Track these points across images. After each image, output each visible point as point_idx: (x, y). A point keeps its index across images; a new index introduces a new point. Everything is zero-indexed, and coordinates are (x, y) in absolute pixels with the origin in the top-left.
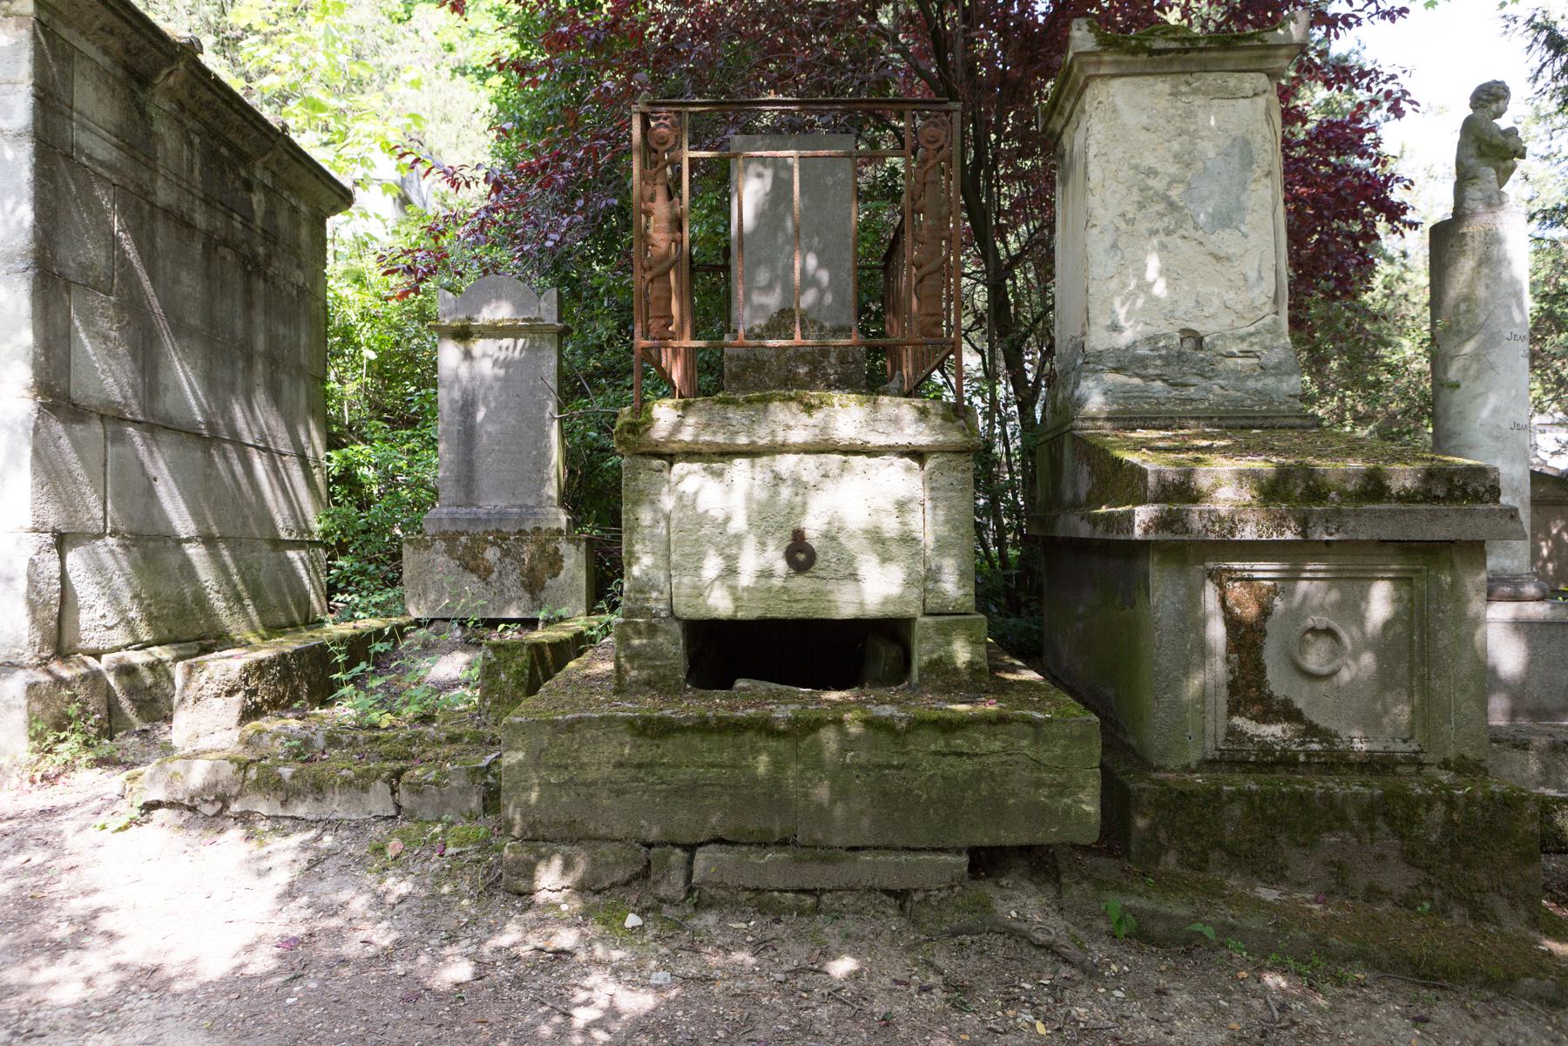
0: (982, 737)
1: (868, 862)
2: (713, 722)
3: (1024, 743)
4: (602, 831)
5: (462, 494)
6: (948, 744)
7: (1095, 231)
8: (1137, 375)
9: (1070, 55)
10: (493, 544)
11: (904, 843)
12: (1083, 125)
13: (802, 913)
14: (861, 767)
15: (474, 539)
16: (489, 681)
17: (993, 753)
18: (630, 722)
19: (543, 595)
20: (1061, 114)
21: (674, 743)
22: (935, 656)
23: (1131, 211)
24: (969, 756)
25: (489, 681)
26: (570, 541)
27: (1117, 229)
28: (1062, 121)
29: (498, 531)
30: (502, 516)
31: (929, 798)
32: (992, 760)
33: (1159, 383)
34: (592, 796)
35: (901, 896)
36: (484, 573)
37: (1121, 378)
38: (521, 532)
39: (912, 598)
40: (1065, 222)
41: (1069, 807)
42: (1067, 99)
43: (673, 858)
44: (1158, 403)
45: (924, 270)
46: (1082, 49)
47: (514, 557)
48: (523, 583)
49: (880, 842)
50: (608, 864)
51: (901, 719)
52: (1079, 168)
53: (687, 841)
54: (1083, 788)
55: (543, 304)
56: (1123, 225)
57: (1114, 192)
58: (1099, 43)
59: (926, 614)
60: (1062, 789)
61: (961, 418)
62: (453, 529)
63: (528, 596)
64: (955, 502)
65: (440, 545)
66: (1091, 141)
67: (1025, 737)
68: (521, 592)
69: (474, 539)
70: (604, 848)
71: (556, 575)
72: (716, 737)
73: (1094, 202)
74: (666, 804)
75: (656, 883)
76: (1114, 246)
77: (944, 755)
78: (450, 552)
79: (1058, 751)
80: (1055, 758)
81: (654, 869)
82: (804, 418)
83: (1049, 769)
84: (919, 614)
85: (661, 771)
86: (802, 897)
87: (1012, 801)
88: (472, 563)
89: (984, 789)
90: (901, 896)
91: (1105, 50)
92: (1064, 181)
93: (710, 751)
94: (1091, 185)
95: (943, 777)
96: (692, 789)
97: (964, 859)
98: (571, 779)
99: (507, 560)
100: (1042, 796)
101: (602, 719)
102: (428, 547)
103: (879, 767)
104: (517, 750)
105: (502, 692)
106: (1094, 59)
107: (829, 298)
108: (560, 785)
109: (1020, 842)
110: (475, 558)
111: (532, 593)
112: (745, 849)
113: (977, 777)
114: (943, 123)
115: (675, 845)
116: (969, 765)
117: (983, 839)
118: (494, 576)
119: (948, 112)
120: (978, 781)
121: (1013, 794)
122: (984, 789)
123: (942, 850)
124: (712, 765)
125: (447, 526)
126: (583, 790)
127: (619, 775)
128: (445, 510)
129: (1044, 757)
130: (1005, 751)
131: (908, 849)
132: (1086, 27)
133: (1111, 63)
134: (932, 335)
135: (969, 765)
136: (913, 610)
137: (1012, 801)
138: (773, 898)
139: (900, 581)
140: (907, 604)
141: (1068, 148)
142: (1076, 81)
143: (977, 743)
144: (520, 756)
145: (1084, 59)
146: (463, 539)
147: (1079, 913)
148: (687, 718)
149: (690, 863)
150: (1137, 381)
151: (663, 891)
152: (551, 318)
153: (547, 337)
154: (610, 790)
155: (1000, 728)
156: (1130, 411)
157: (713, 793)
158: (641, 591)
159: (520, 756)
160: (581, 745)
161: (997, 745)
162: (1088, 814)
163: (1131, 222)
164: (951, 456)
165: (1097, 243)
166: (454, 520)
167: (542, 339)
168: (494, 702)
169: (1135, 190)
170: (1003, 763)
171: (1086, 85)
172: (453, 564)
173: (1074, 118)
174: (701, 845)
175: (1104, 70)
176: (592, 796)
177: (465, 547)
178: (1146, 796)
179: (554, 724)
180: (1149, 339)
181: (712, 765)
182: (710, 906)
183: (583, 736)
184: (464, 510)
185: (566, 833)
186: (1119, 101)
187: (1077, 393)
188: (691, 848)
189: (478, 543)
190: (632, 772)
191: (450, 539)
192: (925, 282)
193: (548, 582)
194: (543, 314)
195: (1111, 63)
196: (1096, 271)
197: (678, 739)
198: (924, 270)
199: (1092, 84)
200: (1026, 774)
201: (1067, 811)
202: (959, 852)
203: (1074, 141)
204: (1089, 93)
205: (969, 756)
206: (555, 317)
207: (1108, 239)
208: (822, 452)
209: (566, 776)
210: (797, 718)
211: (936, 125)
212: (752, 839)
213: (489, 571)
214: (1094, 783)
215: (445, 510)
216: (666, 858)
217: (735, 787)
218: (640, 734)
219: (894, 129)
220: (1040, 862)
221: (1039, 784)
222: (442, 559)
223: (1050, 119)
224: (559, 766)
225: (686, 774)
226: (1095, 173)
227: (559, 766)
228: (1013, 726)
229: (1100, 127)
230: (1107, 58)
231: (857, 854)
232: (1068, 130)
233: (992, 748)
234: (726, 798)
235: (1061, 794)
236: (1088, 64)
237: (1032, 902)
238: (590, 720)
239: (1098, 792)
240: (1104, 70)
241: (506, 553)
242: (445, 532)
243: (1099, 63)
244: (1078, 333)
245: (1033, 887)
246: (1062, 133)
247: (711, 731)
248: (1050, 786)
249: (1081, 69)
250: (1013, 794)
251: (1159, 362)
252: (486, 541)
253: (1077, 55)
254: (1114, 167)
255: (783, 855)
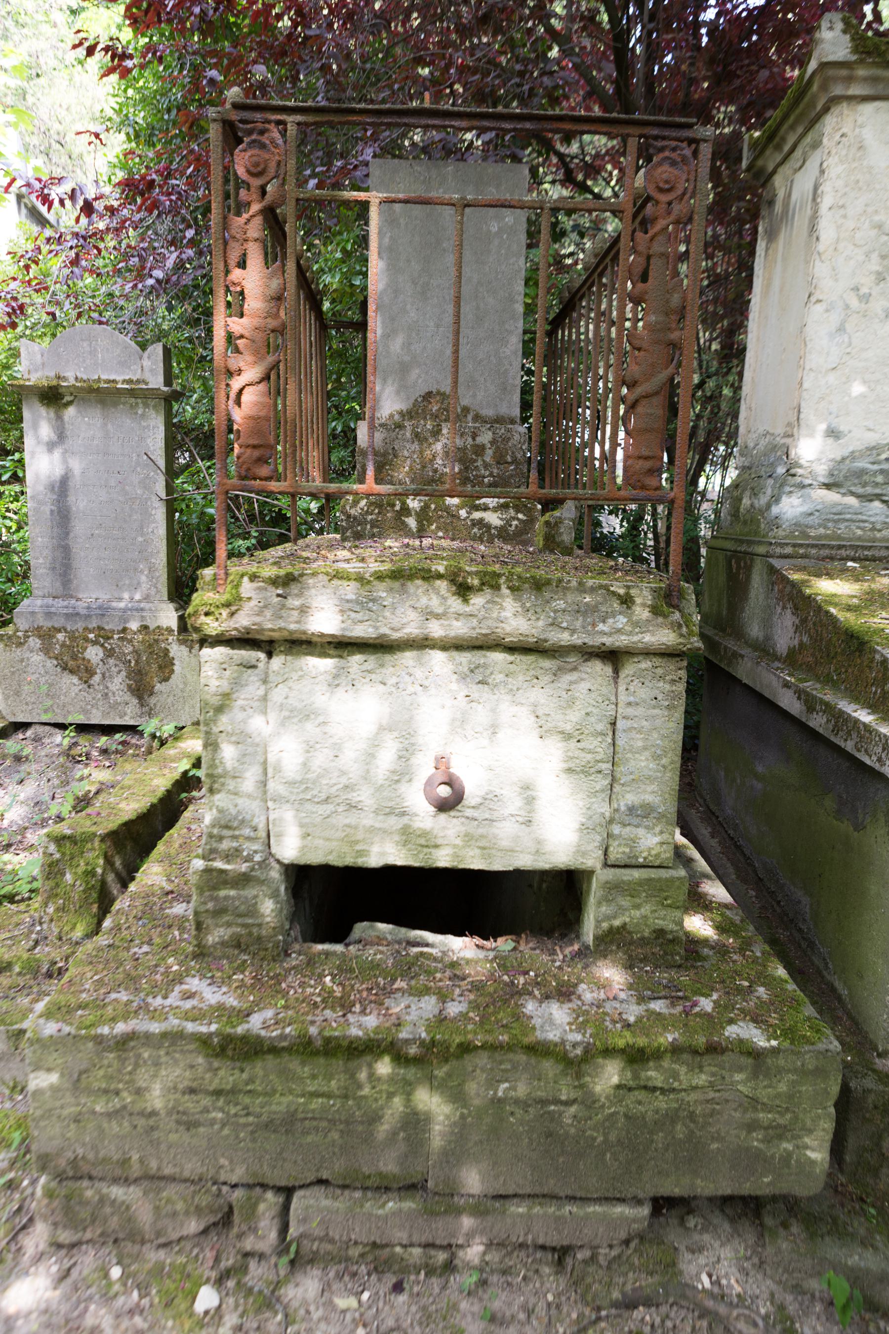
0: (683, 1070)
1: (521, 1216)
2: (319, 1043)
3: (738, 1077)
4: (168, 1171)
5: (58, 584)
6: (636, 1077)
7: (819, 308)
8: (852, 494)
9: (813, 65)
10: (95, 643)
11: (569, 1192)
12: (812, 165)
13: (431, 1271)
14: (517, 1101)
15: (72, 636)
16: (51, 883)
17: (695, 1088)
18: (204, 1041)
19: (152, 701)
20: (779, 147)
21: (259, 1068)
22: (617, 923)
23: (867, 283)
24: (663, 1091)
25: (51, 883)
26: (182, 642)
27: (847, 307)
28: (779, 157)
29: (100, 628)
30: (104, 611)
31: (606, 1141)
32: (693, 1096)
33: (877, 504)
34: (152, 1129)
35: (561, 1254)
36: (85, 672)
37: (832, 497)
38: (124, 630)
39: (590, 847)
40: (767, 286)
41: (789, 1154)
42: (792, 128)
43: (262, 1207)
44: (873, 529)
45: (639, 390)
46: (831, 58)
47: (118, 658)
48: (129, 687)
49: (538, 1190)
50: (175, 1214)
51: (575, 1045)
52: (800, 222)
53: (283, 1183)
54: (810, 1131)
55: (146, 363)
56: (854, 303)
57: (849, 258)
58: (855, 50)
59: (606, 865)
60: (780, 1132)
61: (676, 607)
62: (50, 625)
63: (135, 701)
64: (658, 722)
65: (34, 642)
66: (826, 188)
67: (740, 1069)
68: (128, 697)
69: (72, 636)
70: (170, 1191)
71: (166, 679)
72: (322, 1060)
73: (821, 269)
74: (254, 1140)
75: (240, 1236)
76: (841, 329)
77: (630, 1089)
78: (46, 650)
79: (783, 1087)
80: (778, 1096)
81: (236, 1218)
82: (455, 604)
83: (767, 1108)
84: (598, 866)
85: (247, 1100)
86: (433, 1252)
87: (715, 1146)
88: (71, 663)
89: (680, 1131)
90: (561, 1254)
91: (861, 62)
92: (772, 236)
93: (314, 1077)
94: (821, 247)
95: (626, 1116)
96: (289, 1123)
97: (645, 1211)
98: (124, 1107)
99: (111, 661)
100: (756, 1141)
101: (164, 1035)
102: (20, 644)
103: (544, 1102)
104: (49, 1070)
105: (67, 899)
106: (844, 72)
107: (520, 516)
108: (109, 1115)
109: (720, 1193)
110: (74, 657)
111: (140, 698)
112: (358, 1194)
113: (672, 1117)
114: (684, 159)
115: (264, 1186)
116: (662, 1103)
117: (672, 1188)
118: (97, 678)
119: (692, 141)
120: (673, 1122)
121: (717, 1138)
122: (680, 1131)
123: (621, 1200)
124: (316, 1095)
125: (41, 621)
126: (141, 1122)
127: (189, 1103)
128: (39, 602)
129: (764, 1094)
130: (712, 1085)
131: (572, 1199)
132: (840, 26)
133: (865, 79)
134: (643, 487)
135: (662, 1103)
136: (592, 861)
137: (715, 1146)
138: (393, 1255)
139: (576, 825)
140: (584, 854)
141: (781, 194)
142: (812, 104)
143: (675, 1076)
144: (54, 1078)
145: (831, 72)
146: (60, 636)
147: (786, 1270)
148: (283, 1037)
149: (285, 1209)
150: (852, 501)
151: (249, 1244)
152: (156, 381)
153: (152, 403)
154: (178, 1122)
155: (707, 1059)
156: (839, 538)
157: (317, 1129)
158: (227, 827)
159: (54, 1078)
160: (137, 1066)
161: (702, 1079)
162: (813, 1162)
163: (865, 298)
164: (657, 661)
165: (820, 324)
166: (49, 615)
167: (146, 405)
168: (57, 910)
169: (875, 256)
170: (708, 1101)
171: (826, 110)
172: (50, 664)
173: (798, 153)
174: (302, 1187)
175: (855, 90)
176: (152, 1129)
177: (63, 645)
178: (871, 1099)
179: (99, 1040)
180: (870, 449)
181: (316, 1095)
182: (311, 1261)
183: (139, 1056)
184: (60, 603)
185: (118, 1172)
186: (868, 134)
187: (775, 510)
188: (288, 1192)
189: (77, 641)
190: (206, 1101)
191: (46, 635)
192: (640, 409)
193: (158, 687)
194: (147, 376)
195: (865, 79)
196: (814, 360)
197: (271, 1061)
198: (639, 390)
199: (835, 111)
200: (737, 1115)
201: (786, 1158)
202: (639, 1202)
203: (795, 185)
204: (830, 122)
205: (663, 1091)
206: (161, 379)
207: (835, 318)
208: (480, 648)
209: (116, 1103)
210: (433, 1042)
211: (673, 163)
212: (369, 1183)
213: (91, 672)
214: (826, 1126)
215: (39, 602)
216: (254, 1207)
217: (347, 1123)
218: (217, 1056)
219: (561, 156)
220: (747, 1210)
221: (752, 1126)
222: (37, 658)
223: (762, 152)
224: (106, 1091)
225: (281, 1104)
226: (827, 229)
227: (106, 1091)
228: (726, 1058)
229: (840, 169)
230: (861, 72)
231: (508, 1203)
232: (785, 170)
233: (694, 1083)
234: (335, 1135)
235: (780, 1137)
236: (835, 79)
237: (726, 1253)
238: (148, 1036)
239: (829, 1137)
240: (855, 90)
241: (110, 654)
242: (39, 628)
243: (850, 80)
244: (780, 430)
245: (727, 1226)
246: (774, 172)
247: (316, 1053)
248: (766, 1128)
249: (824, 87)
250: (717, 1138)
251: (880, 479)
252: (86, 639)
253: (823, 66)
254: (851, 224)
255: (408, 1205)
